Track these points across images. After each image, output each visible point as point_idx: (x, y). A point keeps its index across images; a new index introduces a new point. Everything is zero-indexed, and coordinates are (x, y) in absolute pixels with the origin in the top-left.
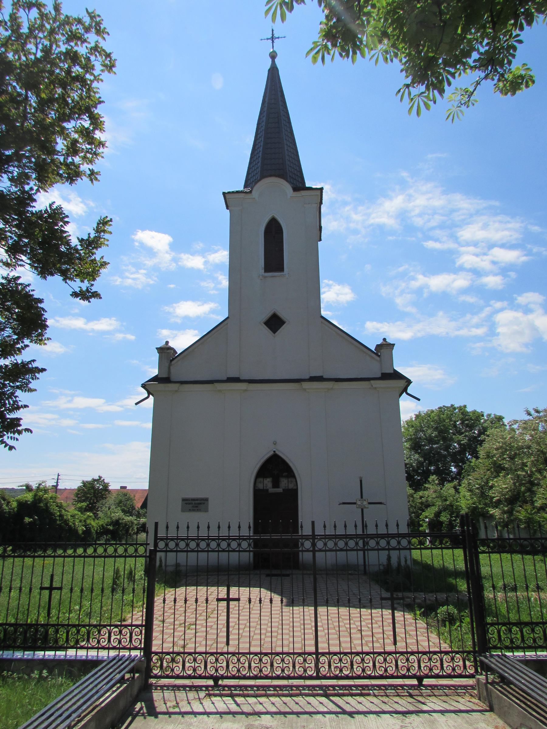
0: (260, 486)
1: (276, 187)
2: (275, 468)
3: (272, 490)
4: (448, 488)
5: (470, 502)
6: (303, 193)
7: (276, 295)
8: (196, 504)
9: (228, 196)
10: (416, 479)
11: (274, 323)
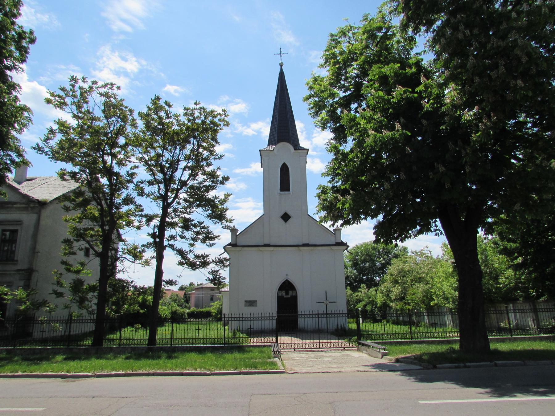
0: (280, 295)
1: (286, 146)
2: (287, 286)
3: (285, 296)
4: (372, 291)
5: (383, 299)
6: (300, 151)
7: (286, 203)
8: (251, 303)
9: (262, 152)
10: (353, 284)
11: (286, 217)
